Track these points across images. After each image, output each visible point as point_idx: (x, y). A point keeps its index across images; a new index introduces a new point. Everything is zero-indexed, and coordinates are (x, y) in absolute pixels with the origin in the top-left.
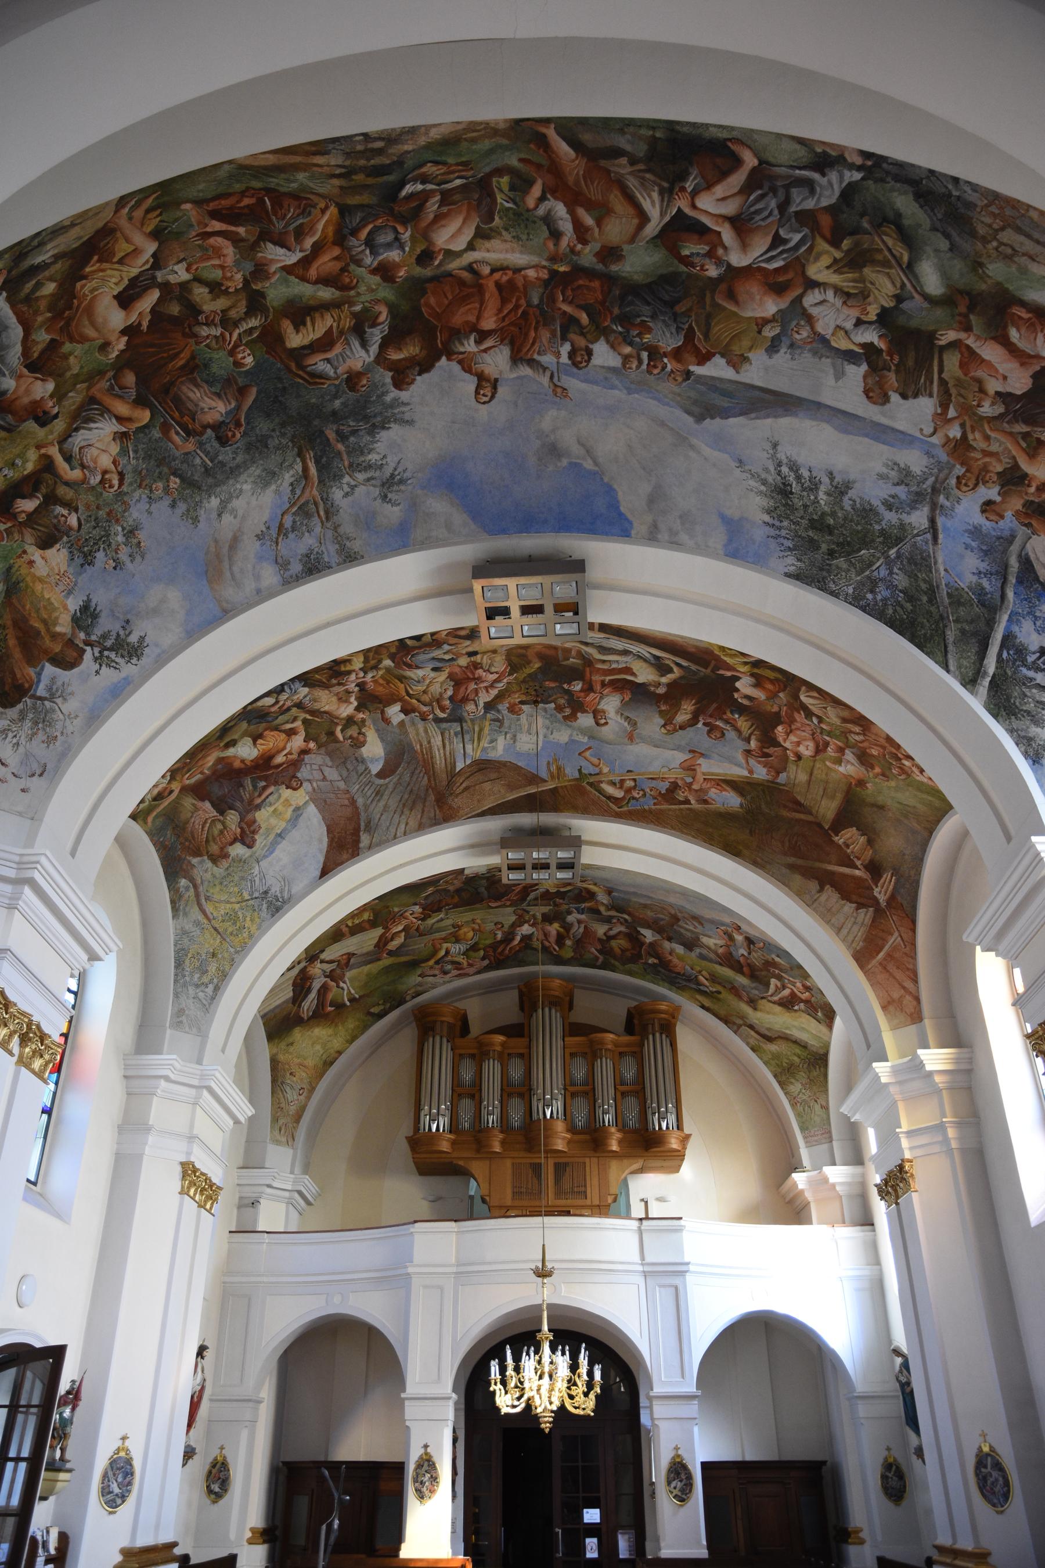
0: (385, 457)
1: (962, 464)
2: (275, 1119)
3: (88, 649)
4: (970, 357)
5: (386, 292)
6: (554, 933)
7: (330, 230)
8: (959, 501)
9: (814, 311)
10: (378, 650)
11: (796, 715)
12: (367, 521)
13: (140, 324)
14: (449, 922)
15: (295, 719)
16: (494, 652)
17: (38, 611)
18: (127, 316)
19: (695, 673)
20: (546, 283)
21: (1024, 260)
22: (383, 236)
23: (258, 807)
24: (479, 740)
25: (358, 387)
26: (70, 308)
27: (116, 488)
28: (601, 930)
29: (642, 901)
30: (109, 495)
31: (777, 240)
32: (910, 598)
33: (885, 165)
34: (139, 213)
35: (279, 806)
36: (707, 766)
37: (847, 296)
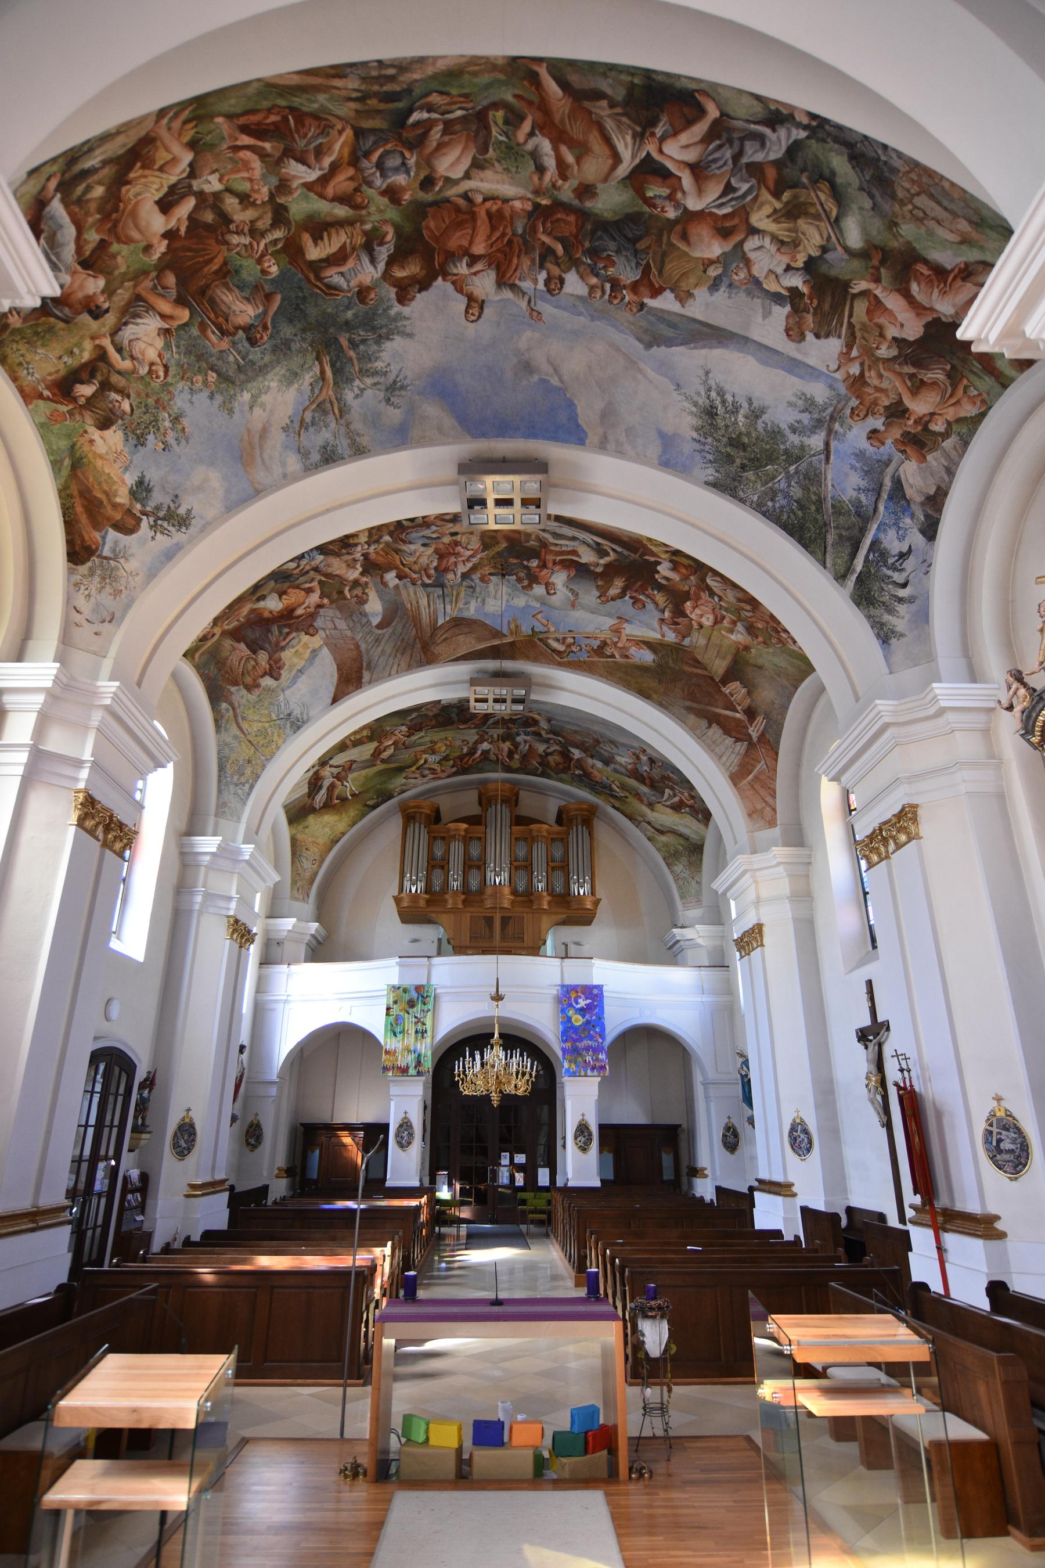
0: (389, 365)
1: (857, 397)
2: (294, 882)
3: (144, 518)
4: (876, 305)
5: (392, 213)
6: (506, 749)
7: (346, 152)
8: (850, 428)
9: (752, 256)
10: (380, 528)
11: (702, 594)
12: (374, 420)
13: (178, 229)
14: (428, 739)
15: (312, 580)
16: (472, 533)
17: (100, 484)
18: (167, 222)
19: (626, 557)
20: (530, 214)
21: (932, 224)
22: (392, 160)
23: (283, 649)
24: (456, 602)
25: (367, 300)
26: (116, 210)
27: (162, 378)
28: (541, 748)
29: (573, 728)
30: (156, 384)
31: (729, 189)
32: (802, 507)
33: (827, 127)
34: (177, 124)
35: (299, 648)
36: (630, 630)
37: (781, 243)
